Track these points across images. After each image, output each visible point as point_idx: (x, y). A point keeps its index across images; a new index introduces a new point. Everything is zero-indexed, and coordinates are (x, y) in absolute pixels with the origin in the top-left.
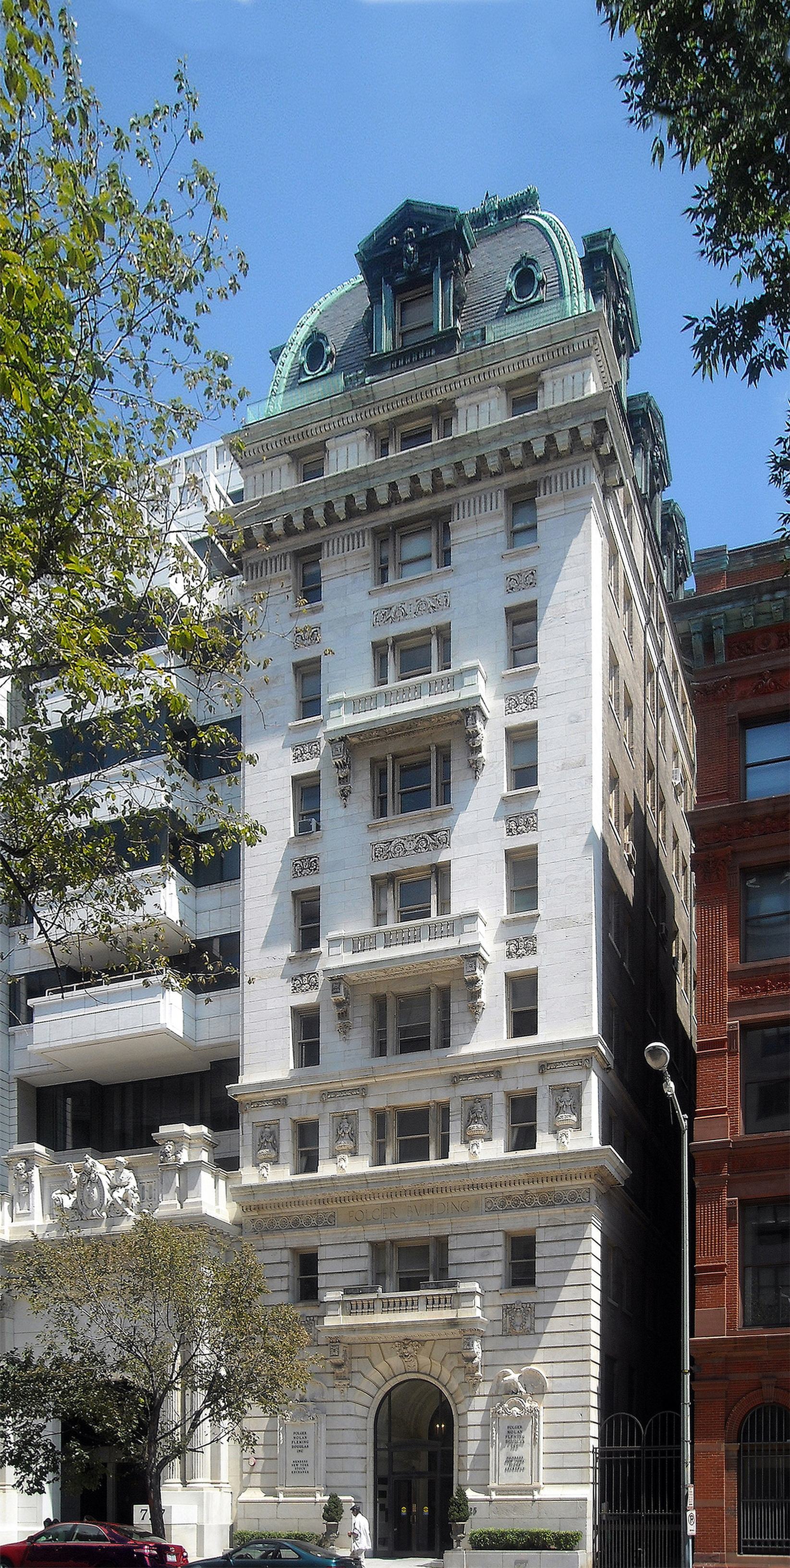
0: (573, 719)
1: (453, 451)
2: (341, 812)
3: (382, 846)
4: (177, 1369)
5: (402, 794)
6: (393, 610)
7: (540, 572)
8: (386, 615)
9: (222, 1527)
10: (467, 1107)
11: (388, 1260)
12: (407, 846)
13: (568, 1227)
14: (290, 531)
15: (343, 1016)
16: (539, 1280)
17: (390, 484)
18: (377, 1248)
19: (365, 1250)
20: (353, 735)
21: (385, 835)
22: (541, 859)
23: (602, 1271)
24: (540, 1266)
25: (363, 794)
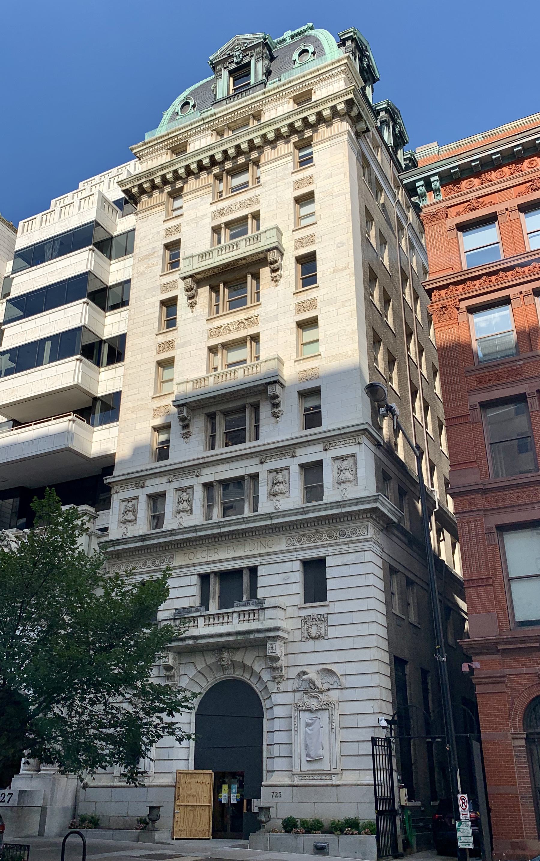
0: (339, 245)
1: (261, 129)
2: (190, 315)
3: (215, 330)
4: (513, 840)
5: (229, 301)
6: (225, 210)
7: (315, 177)
8: (221, 212)
9: (64, 809)
10: (271, 477)
11: (211, 587)
12: (231, 328)
13: (351, 554)
14: (165, 182)
15: (185, 427)
16: (330, 596)
17: (307, 564)
18: (204, 578)
19: (195, 580)
20: (197, 274)
21: (217, 323)
22: (319, 319)
23: (383, 565)
24: (330, 584)
25: (204, 304)
